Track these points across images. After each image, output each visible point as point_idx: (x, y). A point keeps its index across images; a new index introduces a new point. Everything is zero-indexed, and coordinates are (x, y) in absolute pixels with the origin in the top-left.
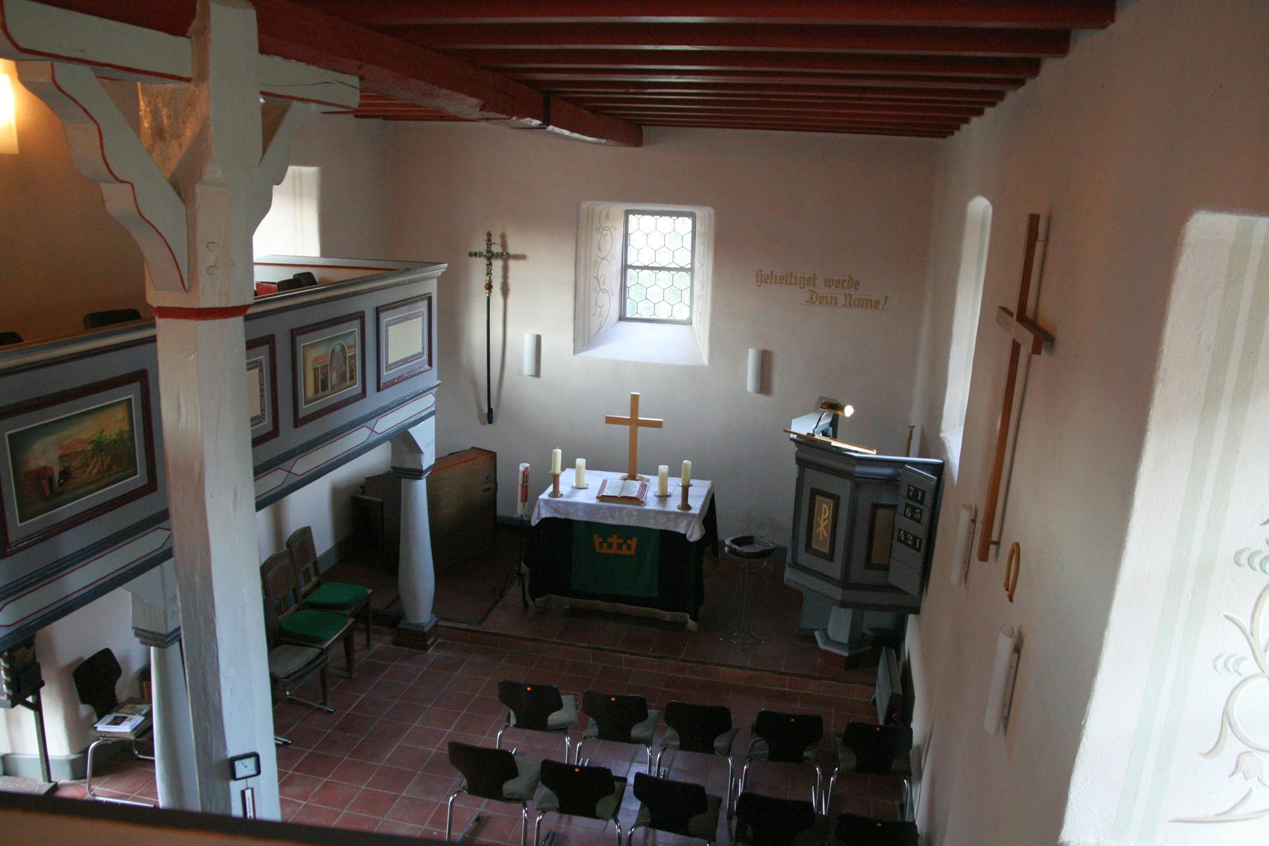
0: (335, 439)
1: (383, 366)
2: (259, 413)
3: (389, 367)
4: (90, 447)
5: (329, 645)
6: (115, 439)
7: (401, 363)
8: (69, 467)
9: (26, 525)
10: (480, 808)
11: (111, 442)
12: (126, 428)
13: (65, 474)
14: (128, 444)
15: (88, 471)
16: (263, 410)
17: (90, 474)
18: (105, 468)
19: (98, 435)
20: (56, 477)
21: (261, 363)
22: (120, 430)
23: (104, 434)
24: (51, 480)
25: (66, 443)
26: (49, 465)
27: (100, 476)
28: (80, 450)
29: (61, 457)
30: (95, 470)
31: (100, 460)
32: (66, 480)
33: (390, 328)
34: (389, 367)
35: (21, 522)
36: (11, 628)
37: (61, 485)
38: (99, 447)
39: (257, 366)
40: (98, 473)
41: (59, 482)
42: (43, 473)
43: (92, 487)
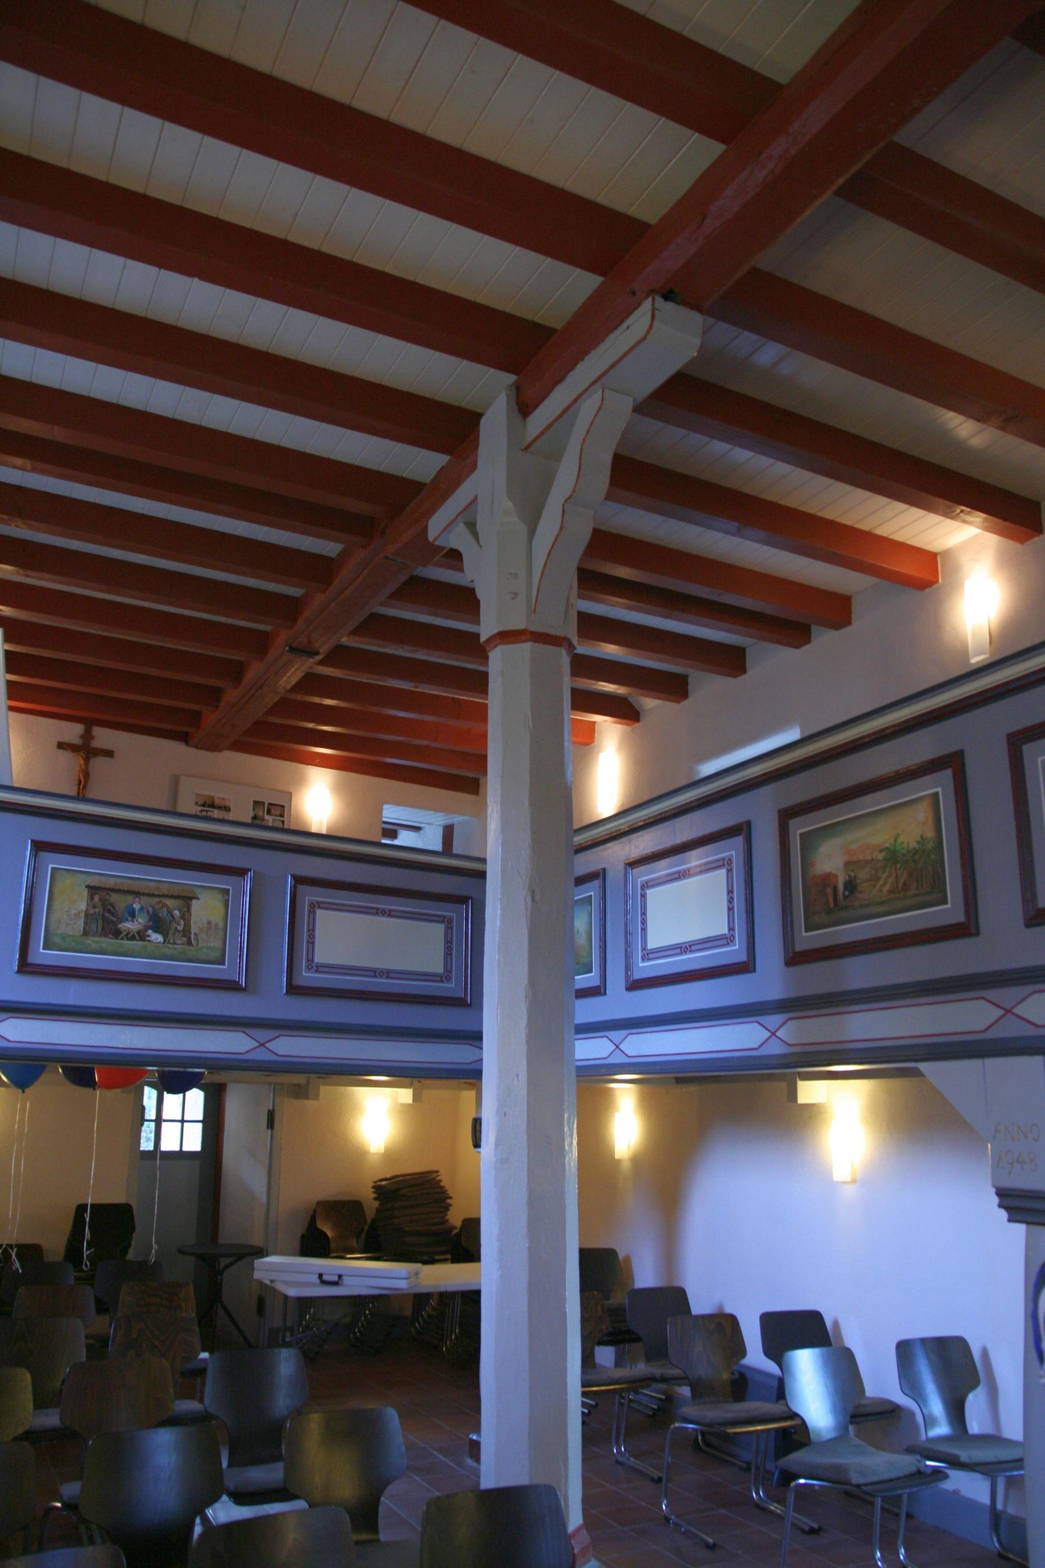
0: (431, 1066)
2: (726, 931)
3: (648, 955)
4: (881, 856)
6: (915, 849)
8: (855, 877)
9: (812, 936)
11: (908, 852)
12: (930, 834)
13: (851, 885)
14: (933, 857)
15: (878, 887)
16: (731, 929)
17: (880, 890)
19: (892, 841)
20: (841, 887)
21: (730, 860)
22: (922, 837)
23: (899, 841)
24: (835, 889)
25: (854, 847)
26: (834, 871)
28: (869, 858)
29: (848, 864)
30: (888, 887)
31: (894, 875)
32: (852, 893)
33: (649, 892)
34: (648, 955)
35: (806, 931)
37: (845, 897)
38: (893, 857)
39: (724, 865)
40: (890, 892)
41: (844, 894)
42: (827, 879)
43: (880, 909)
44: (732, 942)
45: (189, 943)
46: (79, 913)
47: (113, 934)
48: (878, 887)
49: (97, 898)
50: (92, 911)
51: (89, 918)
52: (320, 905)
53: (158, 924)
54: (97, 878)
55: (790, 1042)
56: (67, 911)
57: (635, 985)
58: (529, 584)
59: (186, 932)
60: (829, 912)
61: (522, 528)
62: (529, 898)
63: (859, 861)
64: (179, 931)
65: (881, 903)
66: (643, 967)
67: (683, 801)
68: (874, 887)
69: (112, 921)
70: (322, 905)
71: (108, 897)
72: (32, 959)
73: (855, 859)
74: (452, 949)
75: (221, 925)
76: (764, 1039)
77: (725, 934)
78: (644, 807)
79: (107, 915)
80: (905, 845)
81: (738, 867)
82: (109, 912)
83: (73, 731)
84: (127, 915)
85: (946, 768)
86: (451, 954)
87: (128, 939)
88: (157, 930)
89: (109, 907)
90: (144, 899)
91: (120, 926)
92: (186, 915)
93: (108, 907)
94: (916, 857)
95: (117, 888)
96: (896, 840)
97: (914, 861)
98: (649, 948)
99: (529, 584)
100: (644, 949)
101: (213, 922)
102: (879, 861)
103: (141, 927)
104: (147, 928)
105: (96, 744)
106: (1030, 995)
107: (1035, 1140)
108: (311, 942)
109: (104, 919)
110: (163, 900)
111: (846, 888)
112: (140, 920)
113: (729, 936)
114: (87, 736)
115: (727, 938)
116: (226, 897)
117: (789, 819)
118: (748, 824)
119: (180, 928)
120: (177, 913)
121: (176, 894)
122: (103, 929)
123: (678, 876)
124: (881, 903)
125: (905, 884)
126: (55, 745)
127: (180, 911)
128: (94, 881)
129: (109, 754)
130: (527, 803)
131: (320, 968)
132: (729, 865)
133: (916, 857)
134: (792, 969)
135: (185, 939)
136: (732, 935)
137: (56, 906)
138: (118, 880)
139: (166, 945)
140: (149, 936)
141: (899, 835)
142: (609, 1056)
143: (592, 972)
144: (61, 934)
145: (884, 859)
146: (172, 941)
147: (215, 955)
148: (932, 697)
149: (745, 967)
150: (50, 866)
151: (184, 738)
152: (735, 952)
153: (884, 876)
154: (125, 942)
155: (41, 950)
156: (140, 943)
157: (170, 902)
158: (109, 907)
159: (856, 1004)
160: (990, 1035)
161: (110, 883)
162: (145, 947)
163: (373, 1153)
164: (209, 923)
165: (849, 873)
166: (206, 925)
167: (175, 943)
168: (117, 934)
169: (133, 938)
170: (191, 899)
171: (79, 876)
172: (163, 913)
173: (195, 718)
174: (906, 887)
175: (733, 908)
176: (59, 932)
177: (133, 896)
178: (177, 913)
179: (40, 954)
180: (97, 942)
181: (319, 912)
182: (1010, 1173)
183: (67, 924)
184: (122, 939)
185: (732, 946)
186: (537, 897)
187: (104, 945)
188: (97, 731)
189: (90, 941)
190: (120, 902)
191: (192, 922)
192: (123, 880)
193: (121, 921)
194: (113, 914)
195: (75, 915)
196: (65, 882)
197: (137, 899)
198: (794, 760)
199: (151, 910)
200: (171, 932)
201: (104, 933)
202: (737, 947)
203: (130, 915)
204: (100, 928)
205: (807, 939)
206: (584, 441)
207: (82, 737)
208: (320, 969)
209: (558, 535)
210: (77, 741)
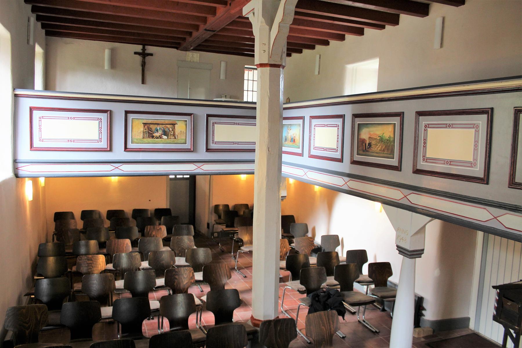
1: (312, 147)
4: (379, 138)
5: (57, 9)
6: (387, 139)
10: (164, 245)
12: (392, 136)
13: (370, 144)
18: (382, 149)
23: (384, 135)
24: (366, 144)
25: (372, 133)
27: (380, 152)
28: (375, 138)
29: (370, 138)
30: (379, 149)
31: (381, 145)
32: (370, 147)
36: (411, 204)
37: (368, 148)
40: (380, 150)
41: (368, 147)
42: (363, 141)
45: (175, 138)
46: (141, 132)
47: (152, 137)
48: (377, 148)
49: (146, 126)
50: (145, 131)
51: (144, 133)
52: (216, 123)
53: (165, 133)
54: (145, 120)
56: (137, 131)
58: (269, 48)
59: (174, 135)
60: (363, 151)
61: (267, 27)
62: (267, 150)
63: (372, 138)
64: (172, 135)
65: (377, 153)
68: (376, 147)
69: (151, 133)
70: (216, 123)
71: (149, 126)
72: (128, 147)
73: (371, 137)
75: (185, 132)
79: (150, 131)
80: (385, 137)
82: (150, 130)
83: (139, 48)
84: (155, 131)
87: (156, 138)
88: (165, 135)
89: (150, 129)
90: (160, 125)
91: (153, 135)
92: (174, 129)
93: (150, 129)
94: (387, 142)
95: (152, 123)
97: (387, 142)
99: (269, 48)
101: (182, 131)
102: (378, 139)
103: (160, 134)
104: (162, 134)
105: (147, 52)
107: (407, 235)
108: (213, 135)
109: (149, 133)
110: (166, 125)
112: (160, 132)
114: (144, 49)
116: (186, 123)
119: (172, 134)
120: (171, 129)
121: (170, 123)
122: (149, 136)
124: (377, 153)
125: (384, 149)
126: (133, 53)
127: (172, 129)
128: (145, 121)
129: (151, 55)
130: (267, 121)
131: (216, 143)
133: (387, 142)
135: (174, 137)
137: (134, 130)
138: (152, 120)
139: (168, 139)
140: (163, 137)
141: (384, 133)
144: (136, 139)
145: (379, 140)
146: (170, 138)
147: (183, 141)
149: (341, 160)
150: (131, 118)
151: (177, 48)
152: (338, 155)
154: (156, 139)
155: (131, 144)
156: (160, 139)
157: (168, 126)
158: (150, 129)
160: (399, 202)
161: (150, 121)
162: (162, 140)
163: (243, 180)
164: (181, 131)
165: (370, 141)
166: (180, 132)
167: (171, 139)
168: (153, 137)
169: (158, 138)
170: (175, 124)
171: (140, 120)
172: (167, 130)
173: (179, 44)
174: (384, 150)
176: (135, 138)
177: (157, 125)
178: (171, 129)
179: (130, 145)
180: (147, 140)
181: (215, 125)
182: (400, 242)
183: (138, 135)
184: (155, 138)
186: (270, 149)
187: (149, 141)
188: (147, 47)
189: (145, 140)
190: (153, 127)
191: (176, 131)
192: (154, 120)
193: (154, 133)
194: (151, 131)
195: (140, 132)
196: (136, 122)
197: (158, 126)
199: (163, 129)
200: (169, 135)
201: (149, 137)
203: (156, 131)
204: (148, 136)
205: (357, 158)
206: (285, 4)
207: (142, 50)
208: (216, 143)
209: (277, 34)
210: (141, 51)
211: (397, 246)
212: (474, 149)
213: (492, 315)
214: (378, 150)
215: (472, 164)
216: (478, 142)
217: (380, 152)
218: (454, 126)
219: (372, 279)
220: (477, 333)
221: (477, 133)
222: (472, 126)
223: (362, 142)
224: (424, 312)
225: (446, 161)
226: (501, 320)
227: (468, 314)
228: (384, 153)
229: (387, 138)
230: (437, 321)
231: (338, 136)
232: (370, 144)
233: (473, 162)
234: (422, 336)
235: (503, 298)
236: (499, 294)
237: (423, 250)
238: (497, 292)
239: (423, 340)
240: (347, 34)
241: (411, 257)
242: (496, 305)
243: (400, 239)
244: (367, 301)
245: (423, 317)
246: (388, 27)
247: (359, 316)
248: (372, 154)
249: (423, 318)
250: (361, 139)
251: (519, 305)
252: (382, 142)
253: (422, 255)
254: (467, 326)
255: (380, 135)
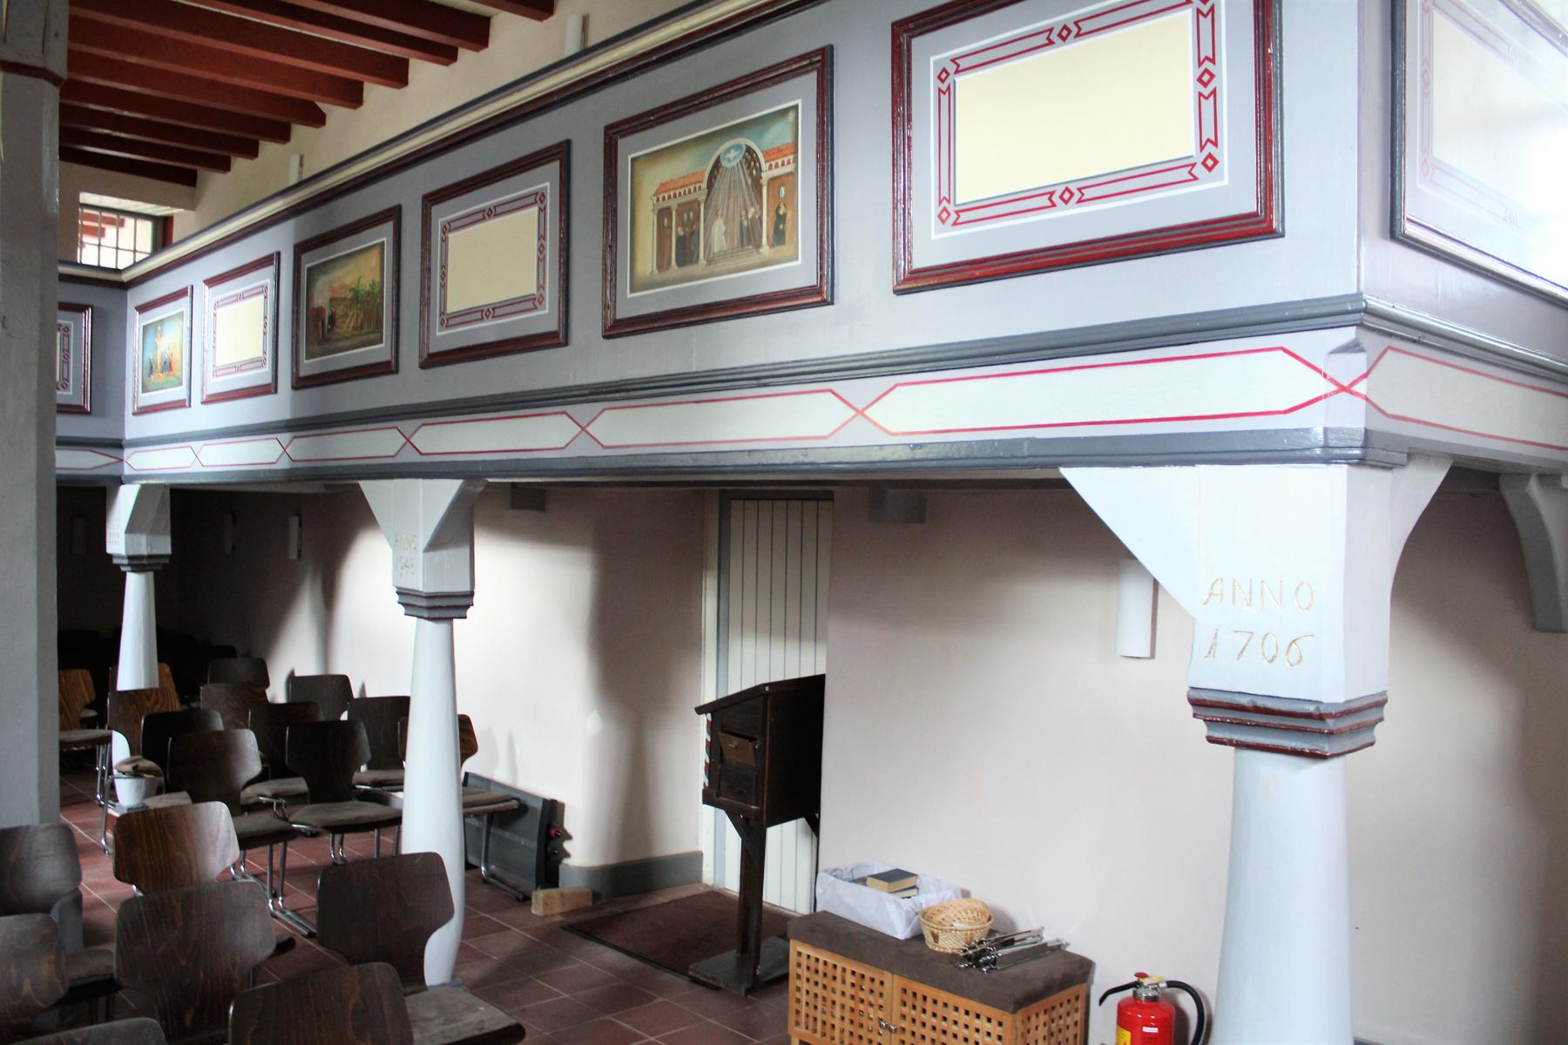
4: (350, 295)
7: (478, 315)
12: (377, 280)
17: (348, 327)
27: (354, 332)
29: (333, 300)
30: (352, 324)
32: (332, 327)
34: (448, 320)
35: (307, 359)
37: (329, 330)
39: (536, 202)
40: (354, 328)
42: (320, 310)
44: (540, 303)
55: (293, 458)
57: (433, 360)
66: (441, 336)
67: (523, 99)
74: (69, 357)
76: (850, 417)
77: (534, 295)
78: (376, 152)
80: (363, 287)
81: (552, 203)
85: (553, 160)
86: (68, 363)
96: (359, 282)
97: (368, 302)
98: (448, 312)
100: (442, 313)
106: (419, 427)
111: (329, 323)
113: (537, 296)
115: (535, 299)
117: (432, 205)
118: (568, 143)
123: (451, 224)
132: (542, 202)
134: (300, 392)
136: (541, 295)
142: (567, 445)
143: (797, 259)
148: (315, 184)
149: (269, 389)
153: (351, 313)
159: (373, 422)
174: (362, 327)
175: (544, 258)
185: (541, 310)
198: (387, 162)
202: (547, 311)
205: (309, 366)
211: (401, 592)
212: (539, 258)
213: (702, 787)
214: (350, 329)
215: (534, 301)
216: (544, 238)
217: (354, 332)
218: (499, 210)
219: (344, 711)
220: (720, 889)
221: (542, 214)
222: (532, 199)
223: (315, 315)
224: (567, 845)
225: (485, 309)
226: (721, 798)
227: (697, 843)
228: (361, 335)
229: (368, 288)
230: (606, 866)
231: (265, 317)
232: (332, 319)
233: (537, 296)
234: (557, 910)
235: (720, 733)
236: (712, 727)
237: (471, 594)
238: (708, 721)
239: (558, 919)
240: (370, 81)
241: (437, 614)
242: (708, 761)
243: (402, 568)
244: (381, 819)
245: (566, 861)
246: (465, 55)
247: (342, 848)
248: (341, 344)
249: (567, 865)
250: (313, 310)
251: (755, 745)
252: (358, 302)
253: (470, 612)
254: (697, 878)
255: (354, 286)
